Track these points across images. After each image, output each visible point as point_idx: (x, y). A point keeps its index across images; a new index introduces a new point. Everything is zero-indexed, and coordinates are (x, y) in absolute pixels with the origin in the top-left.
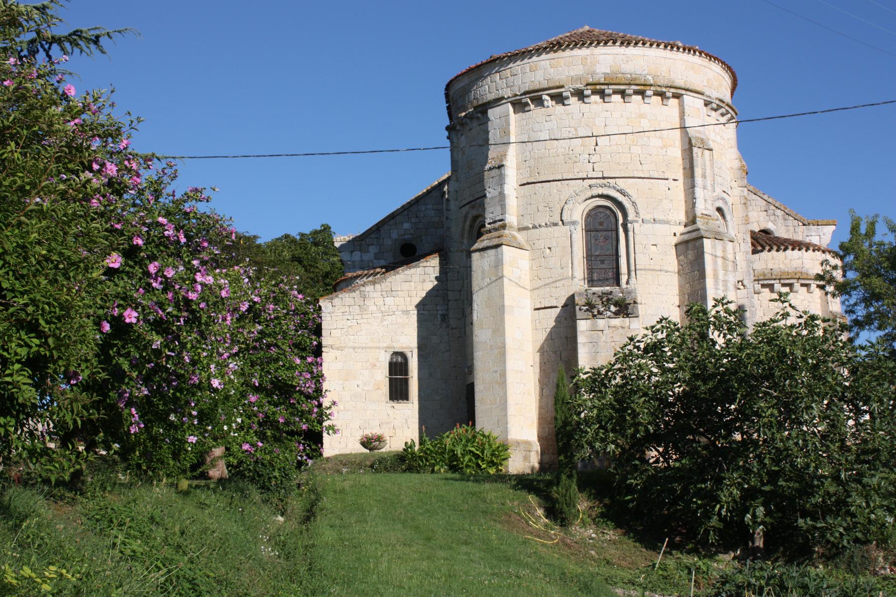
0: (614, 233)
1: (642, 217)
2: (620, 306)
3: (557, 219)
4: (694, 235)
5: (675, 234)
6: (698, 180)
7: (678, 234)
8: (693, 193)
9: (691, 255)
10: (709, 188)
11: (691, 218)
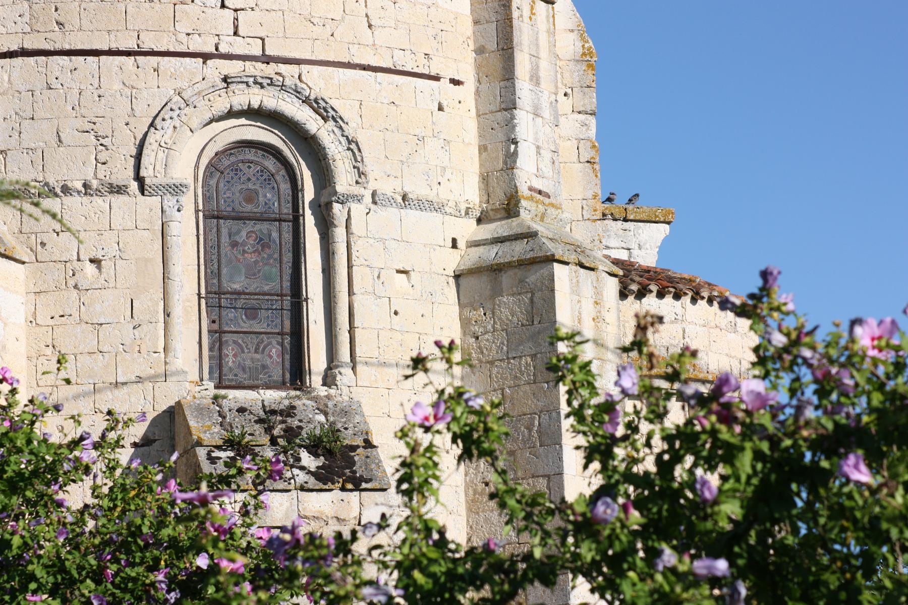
0: (287, 227)
1: (372, 186)
2: (329, 453)
3: (124, 174)
4: (518, 250)
5: (454, 244)
6: (523, 86)
7: (461, 244)
8: (510, 124)
9: (510, 307)
10: (547, 113)
11: (499, 198)
